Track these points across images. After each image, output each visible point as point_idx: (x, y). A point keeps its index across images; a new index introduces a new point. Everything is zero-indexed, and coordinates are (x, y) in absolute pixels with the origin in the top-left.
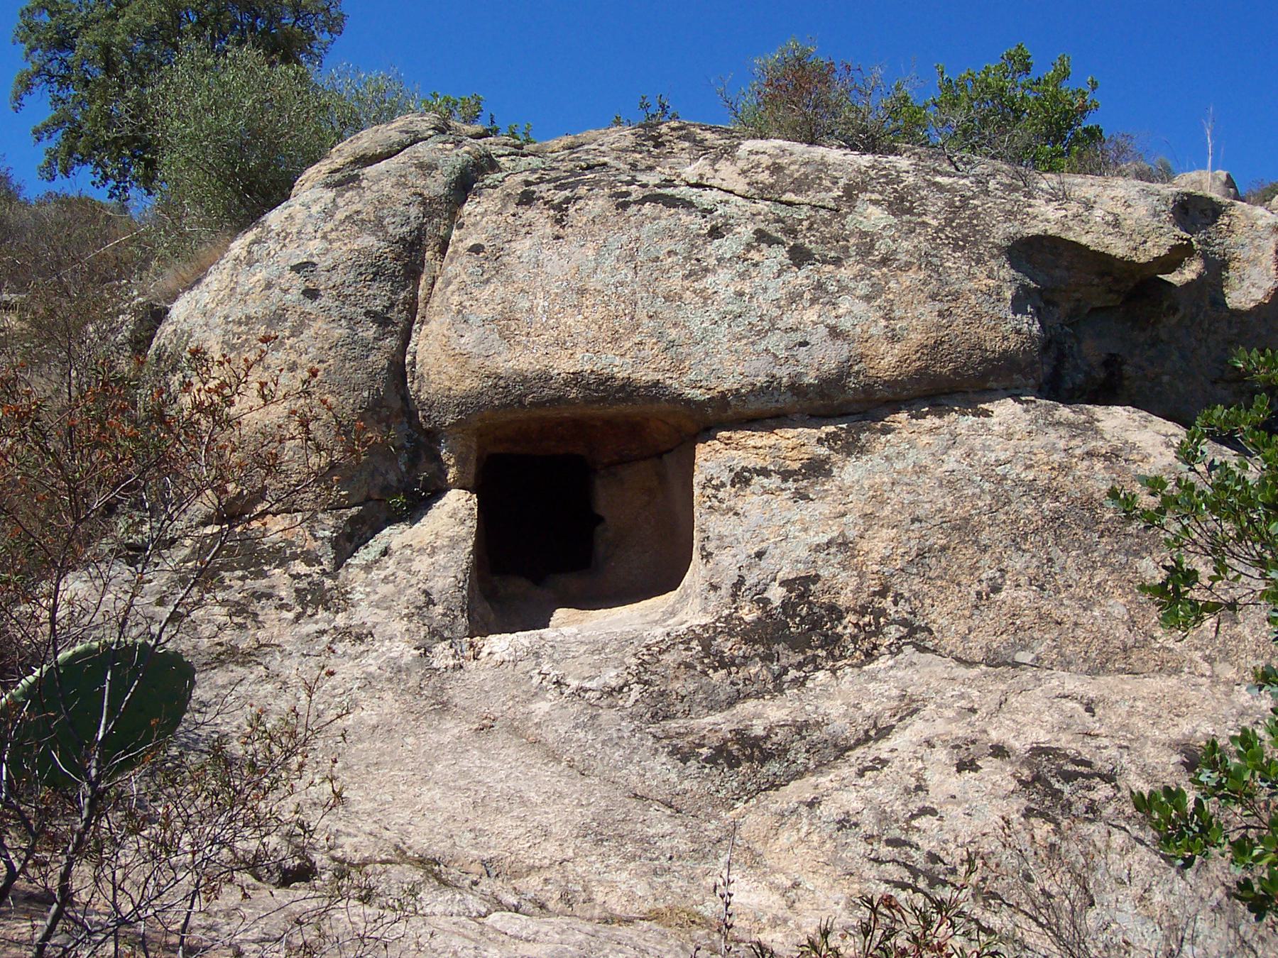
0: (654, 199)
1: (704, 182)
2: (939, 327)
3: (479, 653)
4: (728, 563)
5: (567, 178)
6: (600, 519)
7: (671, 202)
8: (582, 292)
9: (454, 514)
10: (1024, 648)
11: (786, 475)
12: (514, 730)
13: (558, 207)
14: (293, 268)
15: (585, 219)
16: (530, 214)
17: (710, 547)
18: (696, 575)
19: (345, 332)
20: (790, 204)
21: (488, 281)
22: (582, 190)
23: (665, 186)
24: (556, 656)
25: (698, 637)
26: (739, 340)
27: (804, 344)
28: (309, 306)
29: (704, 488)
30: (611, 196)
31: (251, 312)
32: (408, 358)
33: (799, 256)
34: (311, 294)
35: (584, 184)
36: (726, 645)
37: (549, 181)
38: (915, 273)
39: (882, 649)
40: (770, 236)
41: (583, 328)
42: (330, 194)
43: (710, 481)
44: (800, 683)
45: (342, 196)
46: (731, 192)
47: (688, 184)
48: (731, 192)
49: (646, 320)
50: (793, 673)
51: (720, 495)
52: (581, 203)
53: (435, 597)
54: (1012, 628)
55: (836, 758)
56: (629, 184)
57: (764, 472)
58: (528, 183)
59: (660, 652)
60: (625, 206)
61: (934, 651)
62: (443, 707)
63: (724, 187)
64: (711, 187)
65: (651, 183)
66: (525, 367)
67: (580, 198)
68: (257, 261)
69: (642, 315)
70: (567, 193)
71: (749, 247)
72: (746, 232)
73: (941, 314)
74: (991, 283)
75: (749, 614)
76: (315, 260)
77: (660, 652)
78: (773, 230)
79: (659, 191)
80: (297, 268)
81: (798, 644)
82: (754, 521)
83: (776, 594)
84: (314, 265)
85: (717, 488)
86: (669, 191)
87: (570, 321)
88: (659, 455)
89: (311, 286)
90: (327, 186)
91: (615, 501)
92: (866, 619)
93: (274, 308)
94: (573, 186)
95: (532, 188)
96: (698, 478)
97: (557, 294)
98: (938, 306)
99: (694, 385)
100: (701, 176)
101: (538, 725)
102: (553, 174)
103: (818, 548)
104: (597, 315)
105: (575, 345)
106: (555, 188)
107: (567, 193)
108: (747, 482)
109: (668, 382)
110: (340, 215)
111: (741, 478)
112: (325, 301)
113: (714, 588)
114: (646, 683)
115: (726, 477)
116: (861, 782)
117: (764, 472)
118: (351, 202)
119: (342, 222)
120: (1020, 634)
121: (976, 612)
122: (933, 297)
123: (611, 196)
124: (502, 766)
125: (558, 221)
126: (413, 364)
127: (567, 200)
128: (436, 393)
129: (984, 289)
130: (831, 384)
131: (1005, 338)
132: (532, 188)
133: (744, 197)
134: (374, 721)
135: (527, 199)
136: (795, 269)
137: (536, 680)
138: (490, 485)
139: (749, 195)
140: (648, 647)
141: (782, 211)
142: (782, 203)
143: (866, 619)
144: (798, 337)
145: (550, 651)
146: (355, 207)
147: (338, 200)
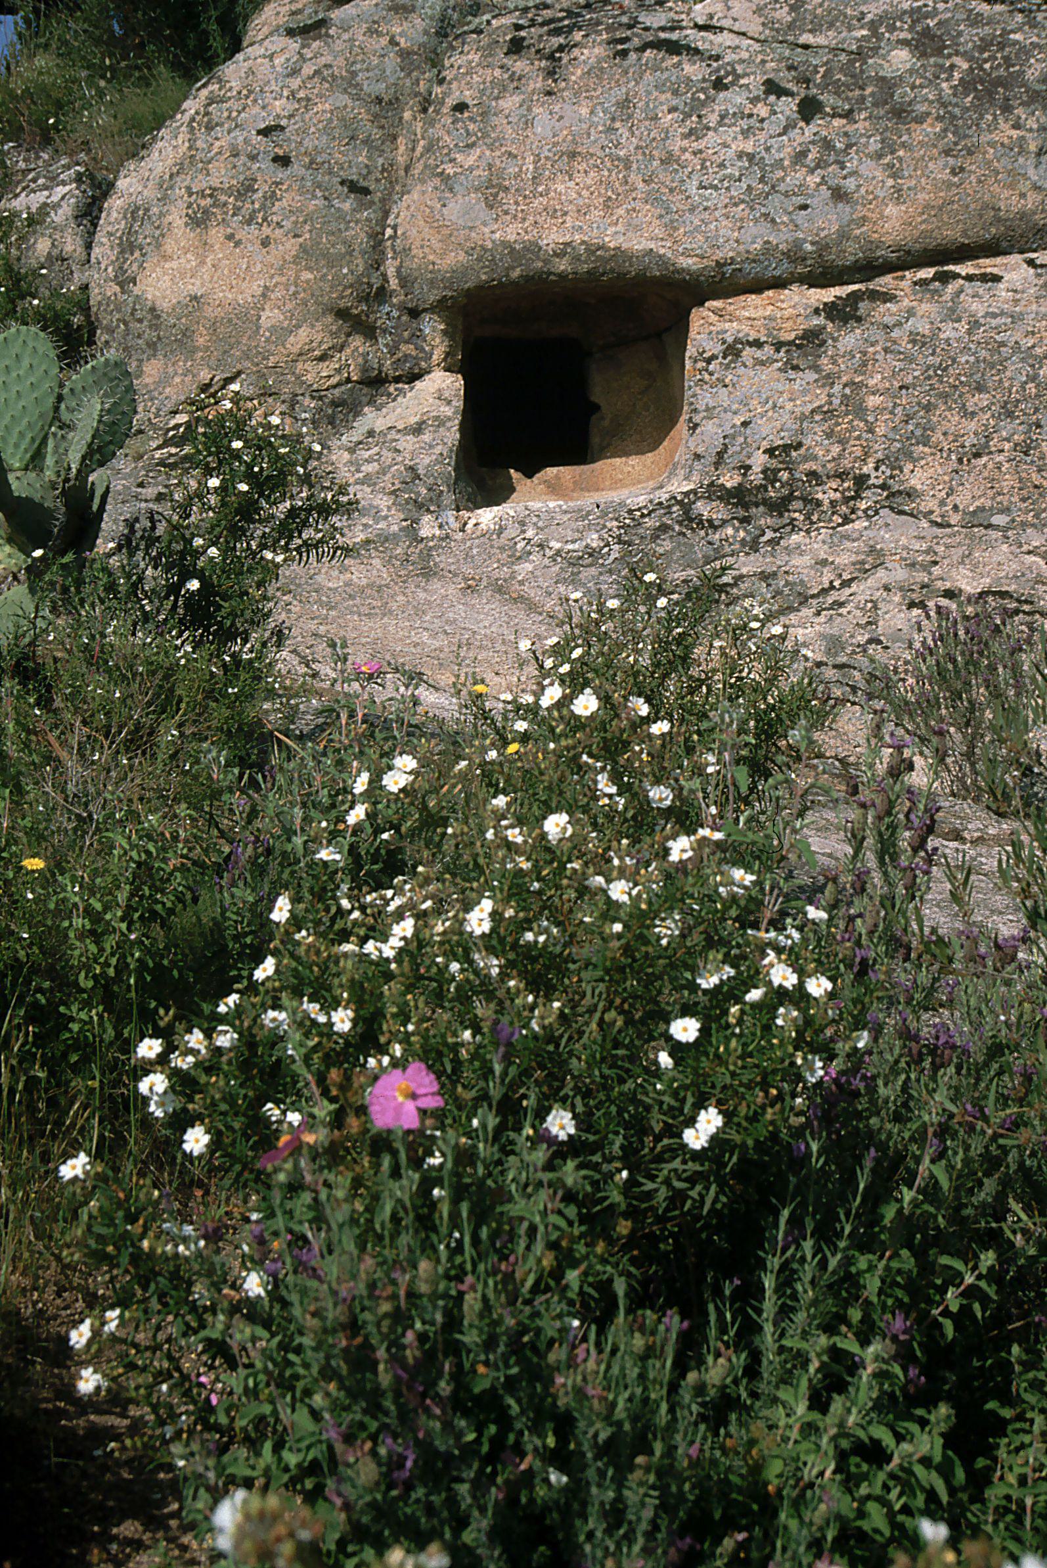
0: (657, 45)
1: (714, 22)
2: (949, 185)
3: (465, 524)
4: (711, 432)
5: (561, 19)
6: (597, 408)
7: (674, 48)
8: (573, 155)
9: (439, 392)
10: (1001, 512)
11: (778, 346)
12: (499, 589)
13: (551, 57)
14: (259, 132)
15: (579, 72)
16: (520, 65)
17: (697, 419)
18: (681, 442)
19: (320, 203)
20: (806, 47)
21: (473, 145)
22: (578, 36)
23: (672, 29)
24: (540, 524)
25: (680, 503)
26: (736, 205)
27: (804, 207)
28: (281, 174)
29: (696, 361)
30: (609, 43)
31: (215, 182)
32: (389, 232)
33: (809, 109)
34: (283, 161)
35: (580, 29)
36: (703, 508)
37: (542, 25)
38: (932, 125)
39: (860, 513)
40: (778, 86)
41: (575, 196)
42: (294, 45)
43: (701, 354)
44: (774, 542)
45: (309, 46)
46: (744, 34)
47: (696, 26)
48: (744, 34)
49: (641, 185)
50: (769, 535)
51: (711, 367)
52: (576, 52)
53: (421, 472)
54: (990, 493)
55: (801, 604)
56: (630, 27)
57: (757, 344)
58: (518, 27)
59: (643, 516)
60: (624, 54)
61: (912, 515)
62: (428, 573)
63: (735, 29)
64: (722, 29)
65: (655, 26)
66: (512, 238)
67: (575, 46)
68: (217, 125)
69: (635, 178)
70: (561, 40)
71: (754, 101)
72: (754, 82)
73: (953, 173)
74: (1015, 133)
75: (730, 480)
76: (284, 122)
77: (643, 516)
78: (786, 79)
79: (663, 35)
80: (265, 132)
81: (779, 507)
82: (742, 390)
83: (759, 460)
84: (283, 129)
85: (709, 361)
86: (674, 36)
87: (561, 188)
88: (658, 335)
89: (281, 153)
90: (291, 33)
91: (608, 390)
92: (846, 485)
93: (242, 178)
94: (570, 30)
95: (523, 34)
96: (691, 351)
97: (547, 158)
98: (951, 160)
99: (687, 253)
100: (711, 17)
101: (521, 583)
102: (547, 14)
103: (803, 418)
104: (589, 182)
105: (566, 214)
106: (549, 33)
107: (561, 40)
108: (738, 354)
109: (662, 251)
110: (308, 69)
111: (732, 351)
112: (296, 168)
113: (698, 457)
114: (625, 543)
115: (718, 349)
116: (817, 620)
117: (757, 344)
118: (320, 53)
119: (310, 78)
120: (999, 499)
121: (956, 477)
122: (947, 152)
123: (609, 43)
124: (487, 617)
125: (550, 73)
126: (394, 237)
127: (561, 48)
128: (419, 269)
129: (1006, 141)
130: (852, 253)
131: (1023, 195)
132: (523, 34)
133: (758, 41)
134: (364, 582)
135: (516, 47)
136: (802, 124)
137: (520, 546)
138: (478, 362)
139: (762, 37)
140: (630, 512)
141: (799, 56)
142: (797, 45)
143: (846, 485)
144: (800, 200)
145: (535, 519)
146: (323, 61)
147: (305, 51)
